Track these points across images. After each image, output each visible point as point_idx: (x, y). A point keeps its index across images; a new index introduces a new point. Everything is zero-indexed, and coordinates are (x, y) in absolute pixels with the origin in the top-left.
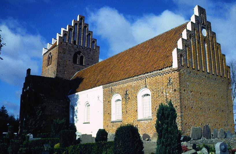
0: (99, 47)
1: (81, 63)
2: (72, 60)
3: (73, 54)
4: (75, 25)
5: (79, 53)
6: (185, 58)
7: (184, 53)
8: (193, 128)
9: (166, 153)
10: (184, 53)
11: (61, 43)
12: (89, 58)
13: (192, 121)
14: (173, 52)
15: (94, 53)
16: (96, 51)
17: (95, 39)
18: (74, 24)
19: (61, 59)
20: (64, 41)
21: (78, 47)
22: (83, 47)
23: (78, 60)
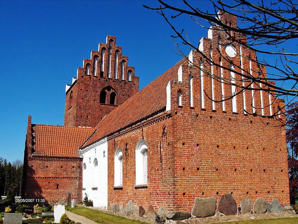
0: (138, 78)
1: (112, 102)
2: (98, 98)
3: (99, 91)
4: (102, 51)
5: (109, 88)
6: (187, 94)
7: (186, 87)
8: (198, 200)
9: (297, 218)
10: (186, 87)
11: (82, 77)
12: (123, 95)
13: (197, 190)
14: (167, 88)
15: (131, 87)
16: (134, 84)
17: (132, 68)
18: (101, 49)
19: (82, 99)
20: (86, 74)
21: (106, 80)
22: (120, 81)
23: (108, 98)
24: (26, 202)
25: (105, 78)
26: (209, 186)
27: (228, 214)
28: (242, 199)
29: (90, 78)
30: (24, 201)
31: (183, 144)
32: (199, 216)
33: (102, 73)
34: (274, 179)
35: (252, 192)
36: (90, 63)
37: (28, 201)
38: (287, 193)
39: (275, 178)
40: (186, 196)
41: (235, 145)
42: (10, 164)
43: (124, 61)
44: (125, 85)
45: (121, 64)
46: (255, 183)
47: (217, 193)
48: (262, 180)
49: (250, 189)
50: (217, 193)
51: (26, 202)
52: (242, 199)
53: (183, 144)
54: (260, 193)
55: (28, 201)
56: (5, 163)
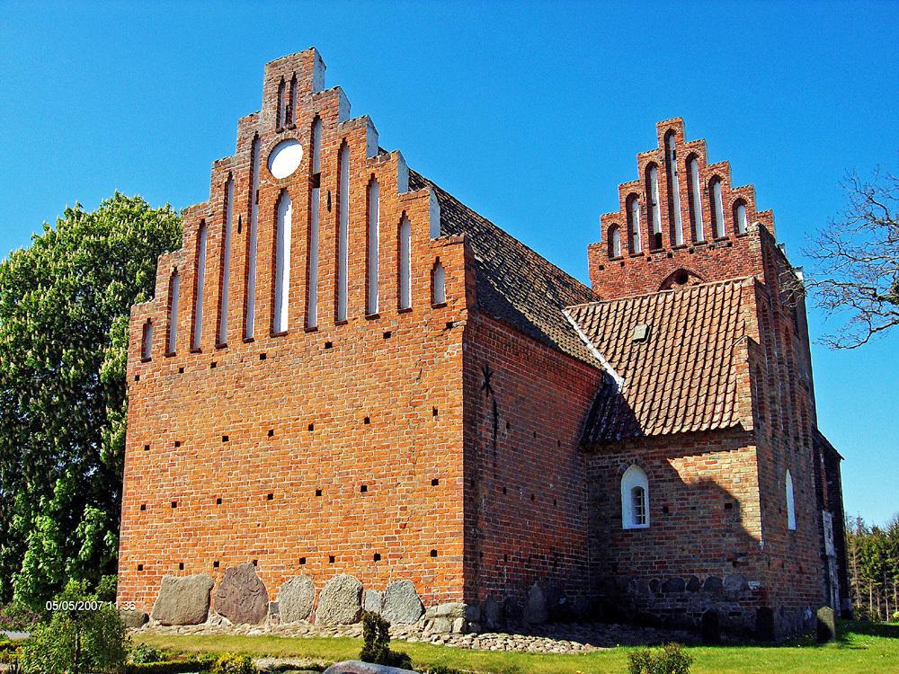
24: (80, 609)
25: (642, 254)
26: (196, 545)
27: (239, 619)
28: (283, 580)
29: (623, 264)
30: (71, 607)
31: (147, 448)
32: (166, 621)
33: (656, 241)
34: (399, 512)
35: (317, 561)
36: (617, 222)
37: (84, 607)
38: (452, 559)
39: (404, 509)
40: (144, 573)
41: (272, 427)
42: (875, 529)
43: (716, 179)
44: (729, 252)
45: (710, 191)
46: (327, 532)
47: (216, 564)
48: (350, 520)
49: (309, 549)
50: (216, 564)
51: (80, 609)
52: (283, 580)
53: (147, 448)
54: (345, 560)
55: (84, 607)
56: (861, 526)
